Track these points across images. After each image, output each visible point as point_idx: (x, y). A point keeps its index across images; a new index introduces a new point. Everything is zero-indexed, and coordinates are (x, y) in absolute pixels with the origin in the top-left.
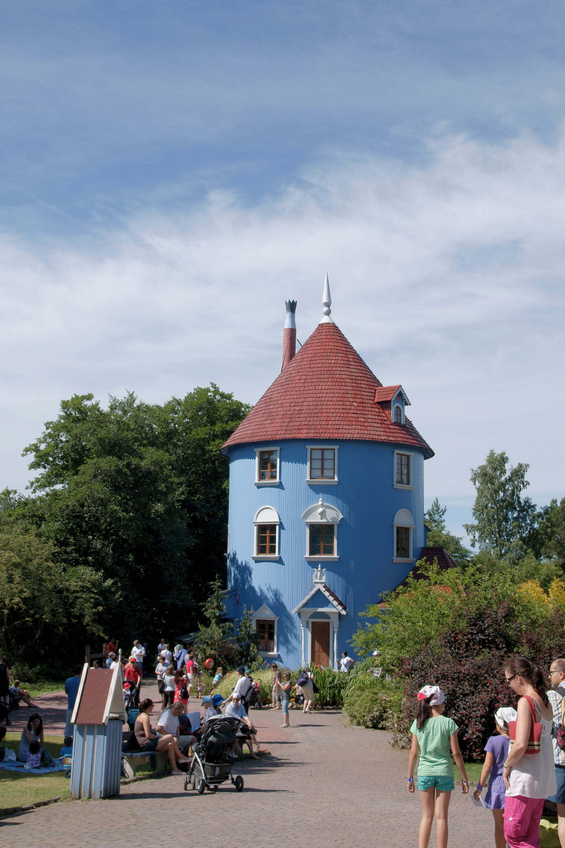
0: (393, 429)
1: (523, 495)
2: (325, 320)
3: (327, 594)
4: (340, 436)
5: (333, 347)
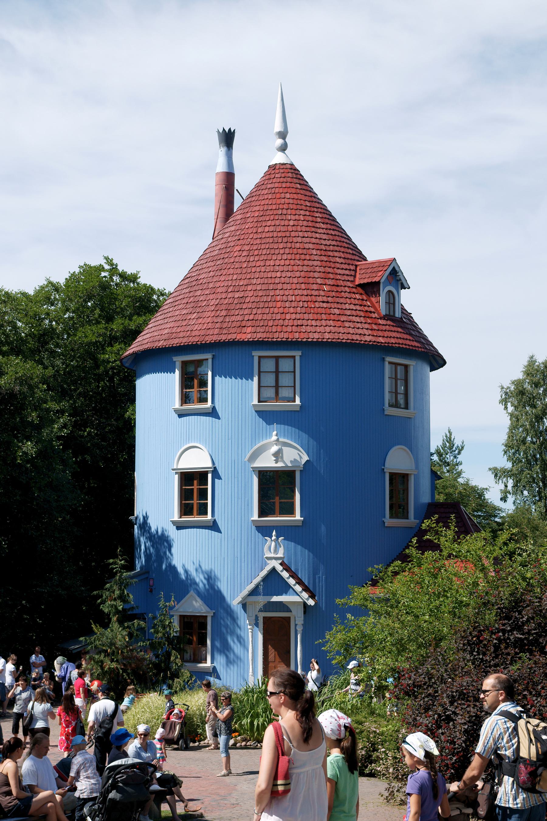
0: (383, 325)
2: (279, 158)
3: (285, 574)
4: (303, 337)
5: (291, 201)
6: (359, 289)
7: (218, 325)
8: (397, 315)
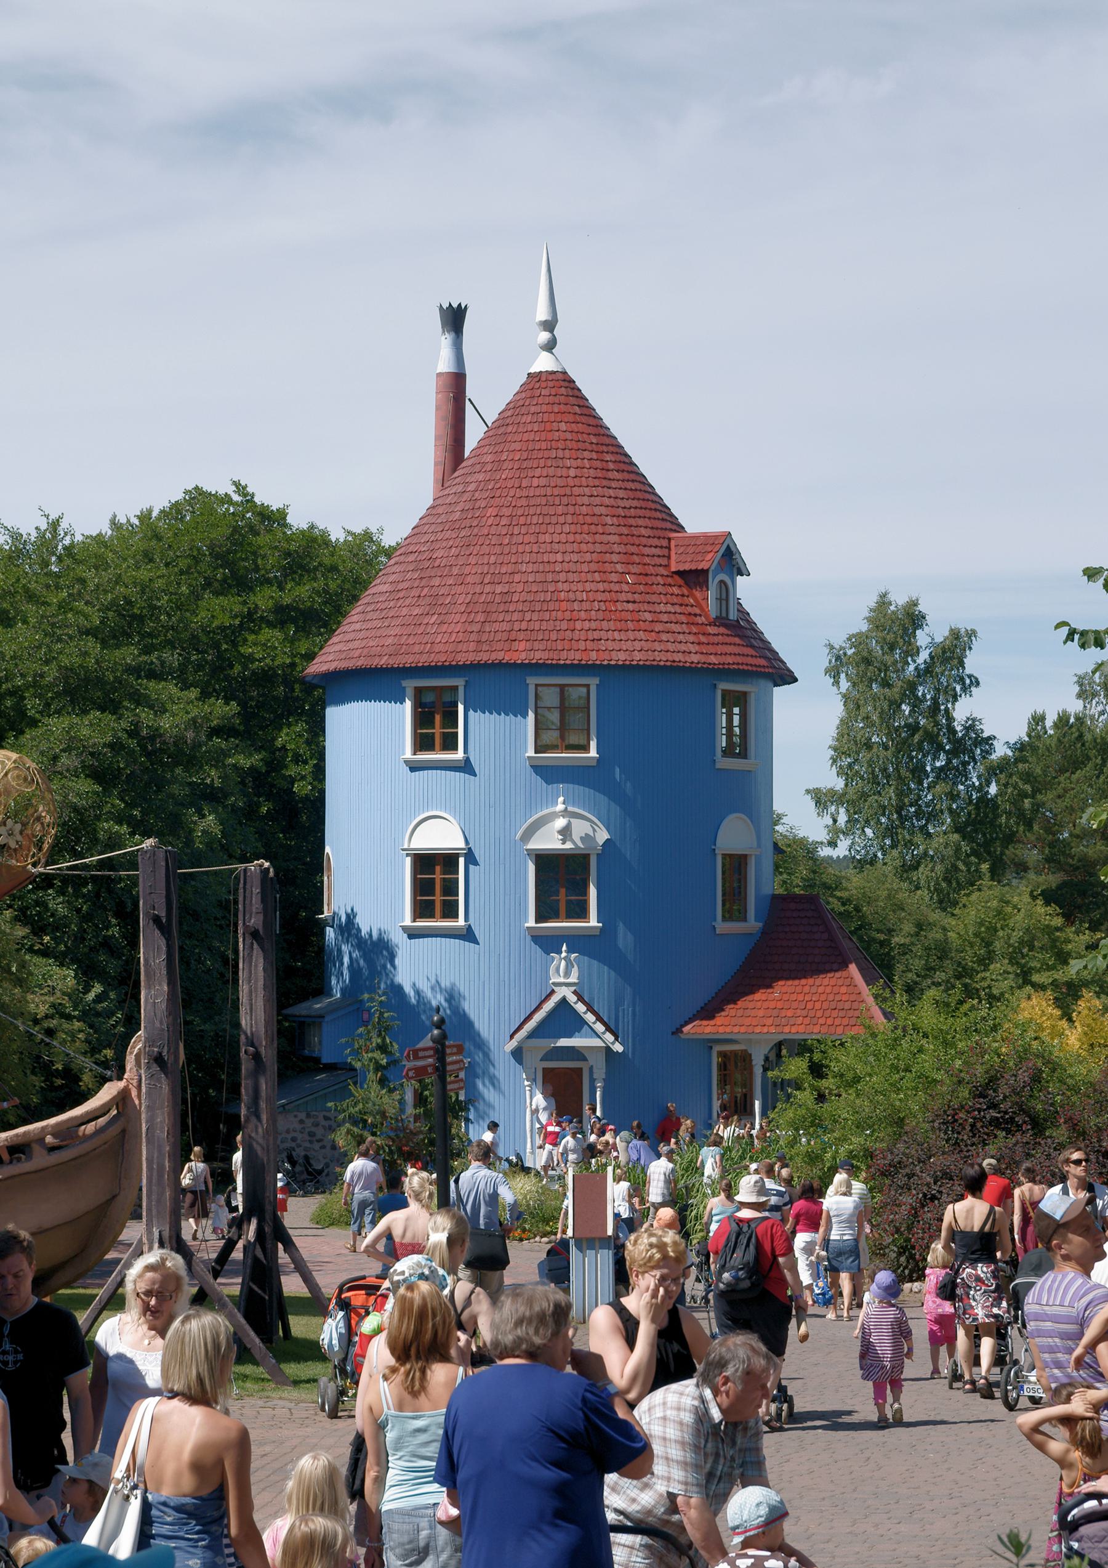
0: (714, 635)
1: (962, 711)
2: (544, 363)
3: (581, 1008)
4: (604, 659)
5: (569, 436)
6: (677, 577)
7: (473, 637)
8: (731, 617)
